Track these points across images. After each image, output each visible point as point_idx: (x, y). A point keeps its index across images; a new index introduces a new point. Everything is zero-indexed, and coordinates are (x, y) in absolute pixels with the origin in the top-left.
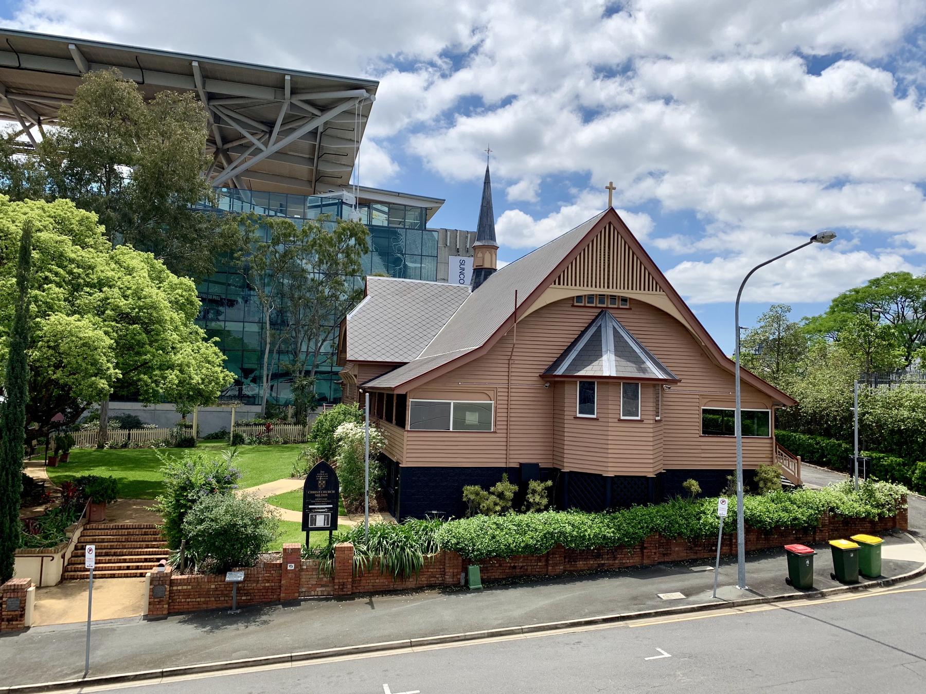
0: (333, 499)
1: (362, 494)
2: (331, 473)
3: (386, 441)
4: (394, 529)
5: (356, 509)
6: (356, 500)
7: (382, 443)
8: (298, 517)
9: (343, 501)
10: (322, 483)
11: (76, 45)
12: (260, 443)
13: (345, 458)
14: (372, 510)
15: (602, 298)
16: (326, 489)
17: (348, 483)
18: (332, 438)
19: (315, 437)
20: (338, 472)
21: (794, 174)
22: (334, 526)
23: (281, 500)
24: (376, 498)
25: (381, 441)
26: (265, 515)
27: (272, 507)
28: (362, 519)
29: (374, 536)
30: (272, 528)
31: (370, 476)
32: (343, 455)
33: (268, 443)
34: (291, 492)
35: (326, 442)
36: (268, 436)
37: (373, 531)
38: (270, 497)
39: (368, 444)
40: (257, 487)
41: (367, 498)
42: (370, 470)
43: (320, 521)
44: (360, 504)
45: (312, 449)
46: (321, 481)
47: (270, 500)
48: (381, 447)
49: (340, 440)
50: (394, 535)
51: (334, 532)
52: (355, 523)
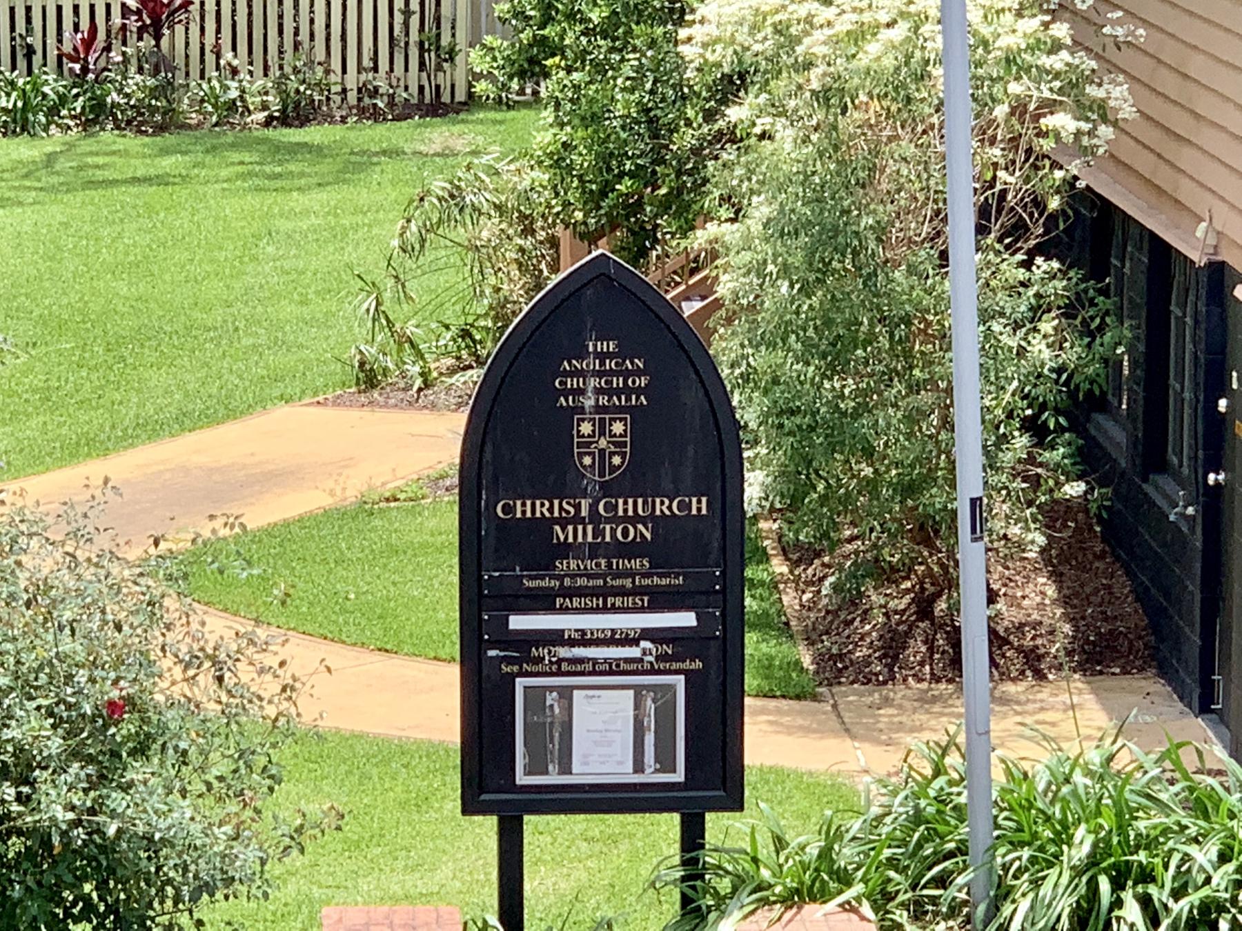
0: (704, 565)
1: (931, 531)
2: (673, 353)
3: (1118, 94)
4: (1201, 806)
5: (892, 647)
6: (887, 575)
7: (1082, 108)
8: (428, 702)
9: (776, 584)
10: (601, 438)
12: (97, 115)
13: (780, 230)
14: (1017, 655)
16: (636, 480)
17: (816, 436)
18: (664, 71)
19: (530, 66)
20: (726, 348)
21: (1185, 181)
22: (711, 773)
23: (282, 570)
24: (1057, 562)
25: (1072, 89)
26: (168, 686)
27: (218, 628)
28: (944, 724)
29: (1044, 861)
30: (230, 789)
31: (991, 377)
32: (760, 210)
33: (157, 118)
34: (365, 509)
35: (623, 105)
36: (159, 64)
37: (1034, 829)
38: (203, 550)
39: (962, 118)
40: (95, 469)
41: (972, 559)
42: (994, 333)
43: (605, 730)
44: (924, 607)
45: (512, 153)
46: (598, 405)
47: (193, 572)
48: (1078, 147)
49: (732, 85)
50: (1205, 855)
51: (716, 825)
52: (884, 760)
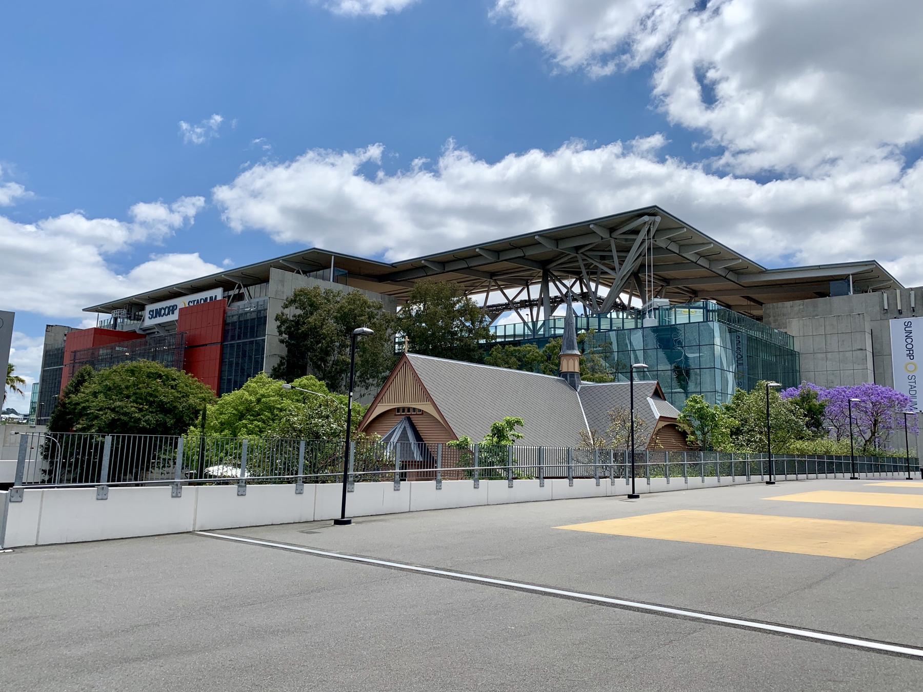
11: (595, 224)
15: (409, 409)
